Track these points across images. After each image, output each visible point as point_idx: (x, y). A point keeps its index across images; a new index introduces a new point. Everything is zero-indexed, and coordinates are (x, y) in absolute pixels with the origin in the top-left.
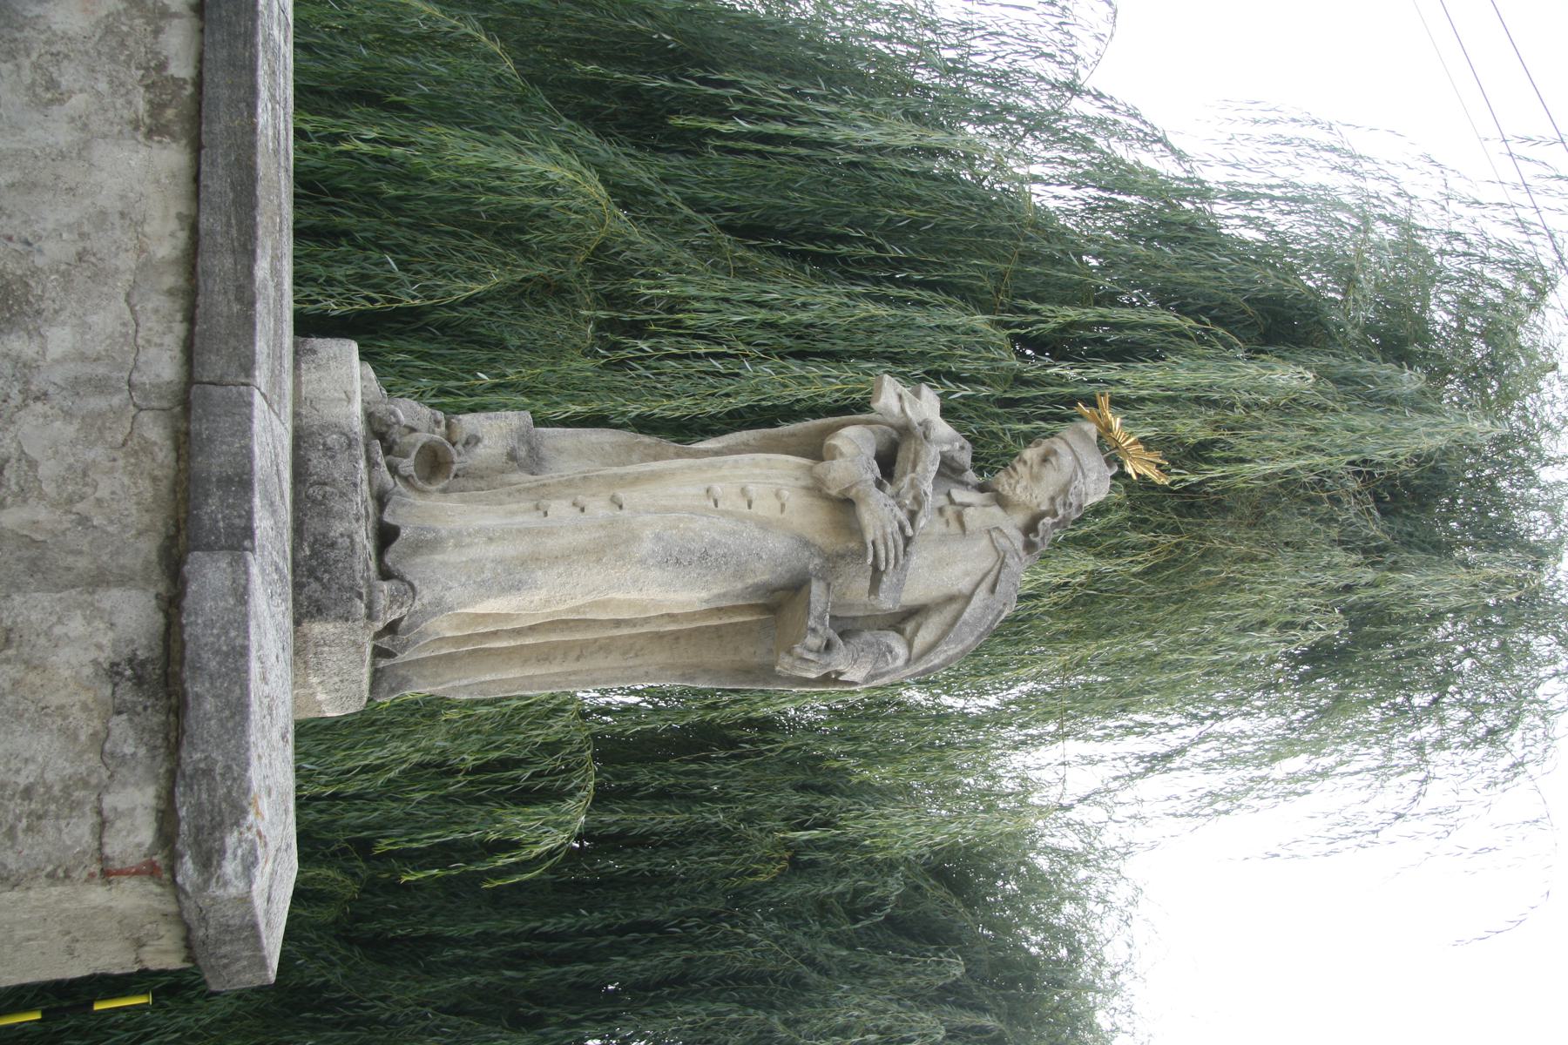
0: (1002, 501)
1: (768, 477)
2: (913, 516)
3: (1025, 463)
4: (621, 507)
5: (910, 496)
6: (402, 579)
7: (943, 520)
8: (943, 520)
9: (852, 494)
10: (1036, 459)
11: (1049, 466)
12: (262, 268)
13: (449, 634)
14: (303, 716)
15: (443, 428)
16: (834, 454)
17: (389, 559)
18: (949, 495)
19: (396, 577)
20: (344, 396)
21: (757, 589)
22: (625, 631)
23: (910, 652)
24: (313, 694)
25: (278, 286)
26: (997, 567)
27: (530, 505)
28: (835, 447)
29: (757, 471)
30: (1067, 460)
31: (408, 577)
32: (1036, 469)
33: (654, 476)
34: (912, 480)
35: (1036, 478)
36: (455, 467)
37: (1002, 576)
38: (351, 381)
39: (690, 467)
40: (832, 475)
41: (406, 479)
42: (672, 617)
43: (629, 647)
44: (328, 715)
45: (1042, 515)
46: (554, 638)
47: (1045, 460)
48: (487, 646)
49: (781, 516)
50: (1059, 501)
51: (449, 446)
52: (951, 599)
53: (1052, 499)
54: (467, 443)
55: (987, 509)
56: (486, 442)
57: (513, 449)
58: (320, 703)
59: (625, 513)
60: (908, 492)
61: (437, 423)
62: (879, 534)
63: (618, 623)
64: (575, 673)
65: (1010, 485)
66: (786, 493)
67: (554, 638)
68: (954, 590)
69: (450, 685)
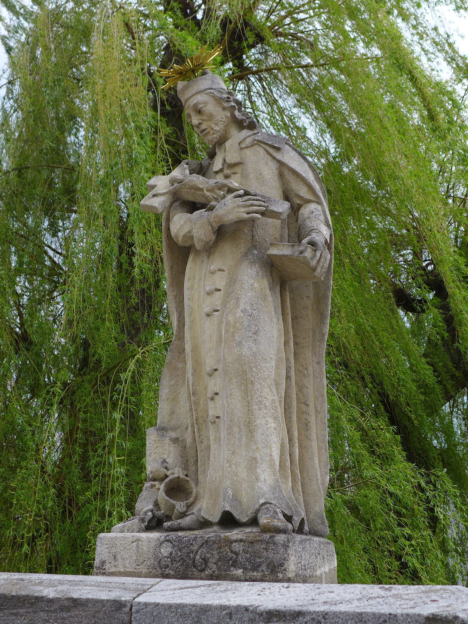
0: (221, 141)
1: (200, 279)
2: (230, 190)
3: (200, 124)
4: (216, 370)
5: (218, 192)
6: (258, 511)
7: (232, 176)
8: (232, 176)
9: (216, 226)
10: (199, 117)
11: (204, 109)
12: (50, 593)
13: (290, 484)
14: (337, 581)
15: (156, 483)
16: (189, 236)
17: (244, 519)
18: (217, 173)
19: (257, 514)
20: (135, 544)
21: (271, 289)
22: (293, 373)
23: (314, 202)
24: (326, 573)
25: (61, 583)
26: (264, 146)
27: (211, 427)
28: (185, 236)
29: (196, 286)
30: (200, 98)
31: (257, 506)
32: (204, 118)
33: (195, 349)
34: (208, 190)
35: (211, 117)
36: (182, 476)
37: (270, 143)
38: (124, 538)
39: (191, 328)
40: (202, 237)
41: (189, 506)
42: (286, 343)
43: (301, 373)
44: (336, 565)
45: (233, 116)
46: (294, 418)
47: (199, 112)
48: (297, 458)
49: (227, 271)
50: (226, 105)
51: (167, 480)
52: (281, 175)
53: (224, 109)
54: (166, 468)
55: (227, 149)
56: (165, 456)
57: (171, 439)
58: (330, 569)
59: (220, 367)
60: (216, 193)
61: (153, 486)
62: (243, 210)
63: (288, 378)
64: (315, 407)
65: (213, 133)
66: (212, 268)
67: (294, 418)
68: (276, 172)
69: (321, 486)
